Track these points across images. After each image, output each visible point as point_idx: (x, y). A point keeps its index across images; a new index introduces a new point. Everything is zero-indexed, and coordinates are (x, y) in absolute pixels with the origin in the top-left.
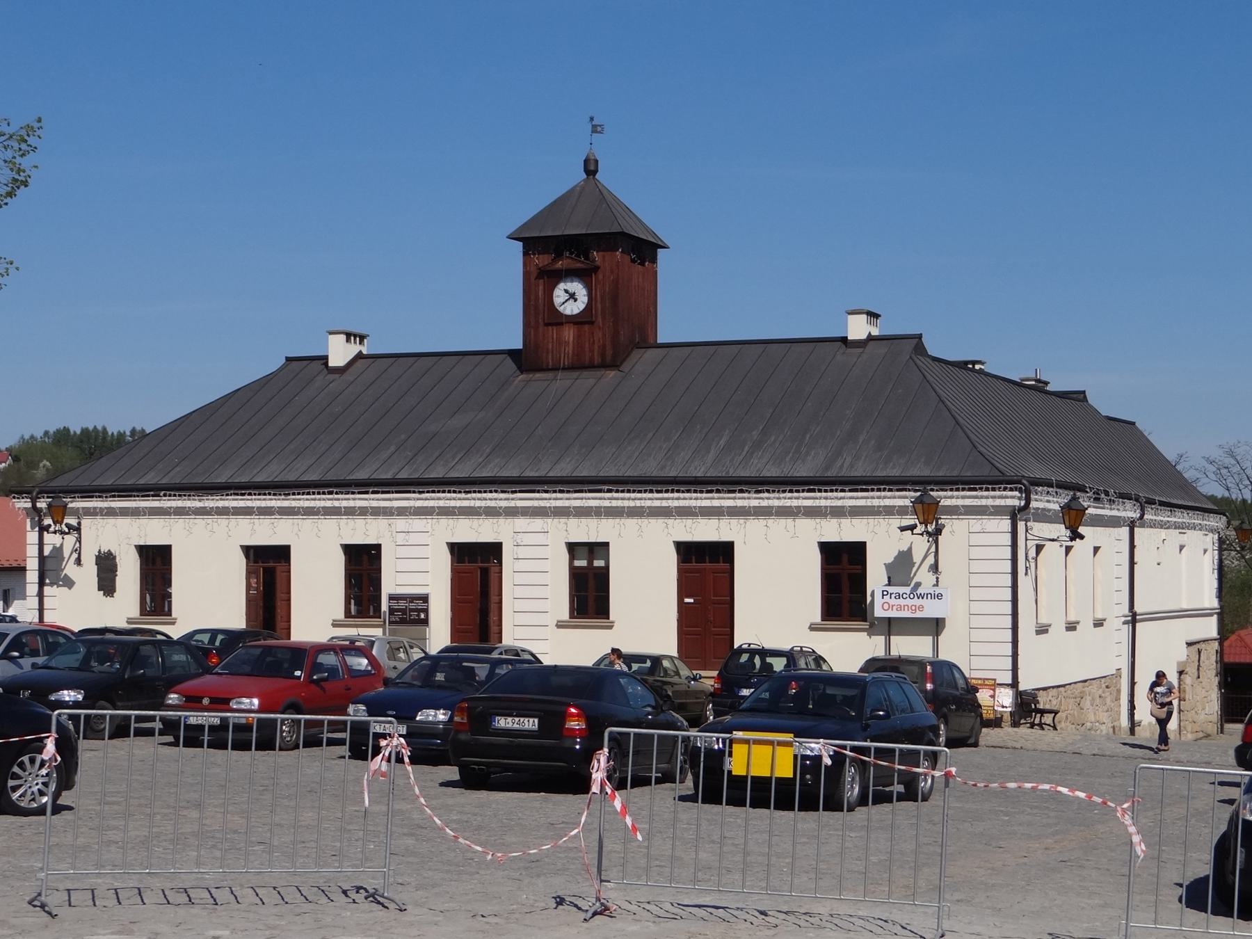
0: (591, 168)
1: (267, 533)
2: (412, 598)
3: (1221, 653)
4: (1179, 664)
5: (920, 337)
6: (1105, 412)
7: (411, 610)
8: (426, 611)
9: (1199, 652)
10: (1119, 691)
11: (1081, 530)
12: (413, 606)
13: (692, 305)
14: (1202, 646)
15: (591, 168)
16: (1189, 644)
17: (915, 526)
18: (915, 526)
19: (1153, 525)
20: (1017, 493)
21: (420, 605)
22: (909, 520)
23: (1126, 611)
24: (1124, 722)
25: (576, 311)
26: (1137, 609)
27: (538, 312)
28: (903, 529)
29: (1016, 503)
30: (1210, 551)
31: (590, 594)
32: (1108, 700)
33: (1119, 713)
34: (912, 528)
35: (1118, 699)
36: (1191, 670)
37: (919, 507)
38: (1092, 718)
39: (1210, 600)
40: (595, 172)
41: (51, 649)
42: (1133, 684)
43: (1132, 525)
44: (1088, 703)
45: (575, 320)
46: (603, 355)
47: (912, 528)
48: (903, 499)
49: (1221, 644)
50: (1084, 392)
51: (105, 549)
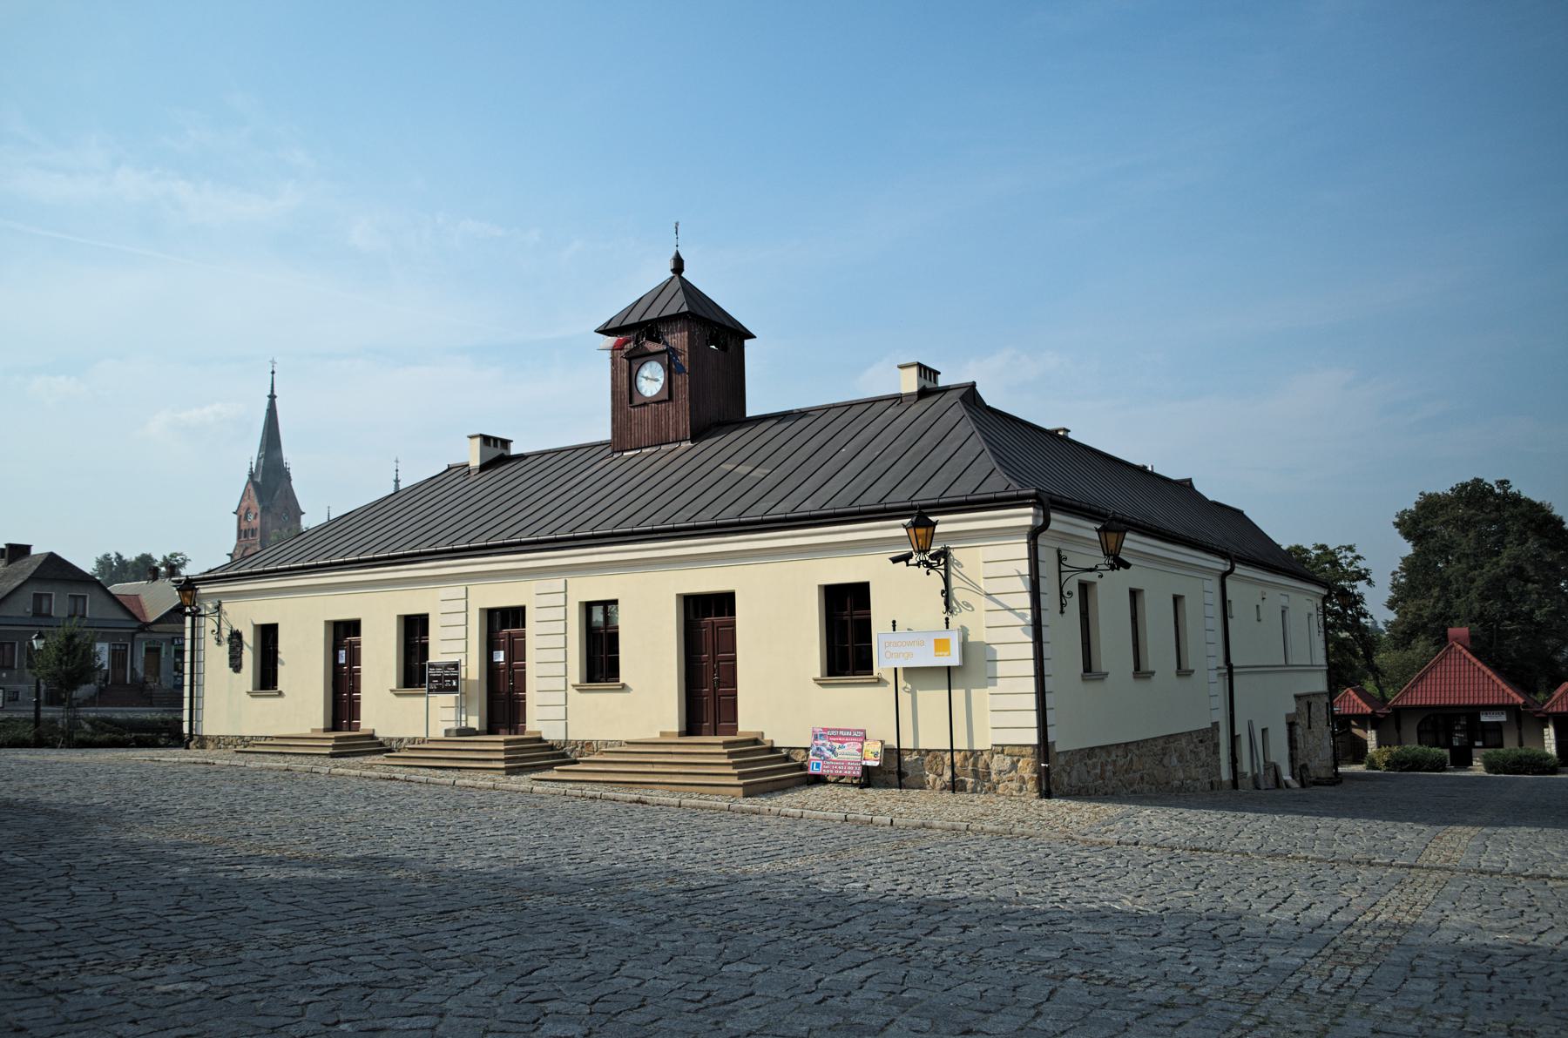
3: (1331, 705)
4: (1288, 716)
5: (974, 385)
8: (456, 678)
9: (1309, 705)
10: (1217, 745)
14: (1312, 699)
16: (1297, 697)
17: (909, 556)
18: (909, 556)
20: (1031, 510)
21: (451, 672)
23: (1222, 664)
24: (1226, 775)
26: (1233, 661)
27: (625, 395)
28: (895, 560)
30: (1314, 617)
31: (601, 657)
32: (1203, 756)
33: (1218, 768)
34: (906, 558)
35: (1216, 751)
36: (1303, 722)
37: (912, 531)
38: (1181, 775)
39: (1321, 659)
42: (1234, 739)
43: (1224, 575)
44: (1175, 759)
45: (657, 401)
46: (677, 431)
47: (906, 558)
48: (896, 529)
49: (1331, 699)
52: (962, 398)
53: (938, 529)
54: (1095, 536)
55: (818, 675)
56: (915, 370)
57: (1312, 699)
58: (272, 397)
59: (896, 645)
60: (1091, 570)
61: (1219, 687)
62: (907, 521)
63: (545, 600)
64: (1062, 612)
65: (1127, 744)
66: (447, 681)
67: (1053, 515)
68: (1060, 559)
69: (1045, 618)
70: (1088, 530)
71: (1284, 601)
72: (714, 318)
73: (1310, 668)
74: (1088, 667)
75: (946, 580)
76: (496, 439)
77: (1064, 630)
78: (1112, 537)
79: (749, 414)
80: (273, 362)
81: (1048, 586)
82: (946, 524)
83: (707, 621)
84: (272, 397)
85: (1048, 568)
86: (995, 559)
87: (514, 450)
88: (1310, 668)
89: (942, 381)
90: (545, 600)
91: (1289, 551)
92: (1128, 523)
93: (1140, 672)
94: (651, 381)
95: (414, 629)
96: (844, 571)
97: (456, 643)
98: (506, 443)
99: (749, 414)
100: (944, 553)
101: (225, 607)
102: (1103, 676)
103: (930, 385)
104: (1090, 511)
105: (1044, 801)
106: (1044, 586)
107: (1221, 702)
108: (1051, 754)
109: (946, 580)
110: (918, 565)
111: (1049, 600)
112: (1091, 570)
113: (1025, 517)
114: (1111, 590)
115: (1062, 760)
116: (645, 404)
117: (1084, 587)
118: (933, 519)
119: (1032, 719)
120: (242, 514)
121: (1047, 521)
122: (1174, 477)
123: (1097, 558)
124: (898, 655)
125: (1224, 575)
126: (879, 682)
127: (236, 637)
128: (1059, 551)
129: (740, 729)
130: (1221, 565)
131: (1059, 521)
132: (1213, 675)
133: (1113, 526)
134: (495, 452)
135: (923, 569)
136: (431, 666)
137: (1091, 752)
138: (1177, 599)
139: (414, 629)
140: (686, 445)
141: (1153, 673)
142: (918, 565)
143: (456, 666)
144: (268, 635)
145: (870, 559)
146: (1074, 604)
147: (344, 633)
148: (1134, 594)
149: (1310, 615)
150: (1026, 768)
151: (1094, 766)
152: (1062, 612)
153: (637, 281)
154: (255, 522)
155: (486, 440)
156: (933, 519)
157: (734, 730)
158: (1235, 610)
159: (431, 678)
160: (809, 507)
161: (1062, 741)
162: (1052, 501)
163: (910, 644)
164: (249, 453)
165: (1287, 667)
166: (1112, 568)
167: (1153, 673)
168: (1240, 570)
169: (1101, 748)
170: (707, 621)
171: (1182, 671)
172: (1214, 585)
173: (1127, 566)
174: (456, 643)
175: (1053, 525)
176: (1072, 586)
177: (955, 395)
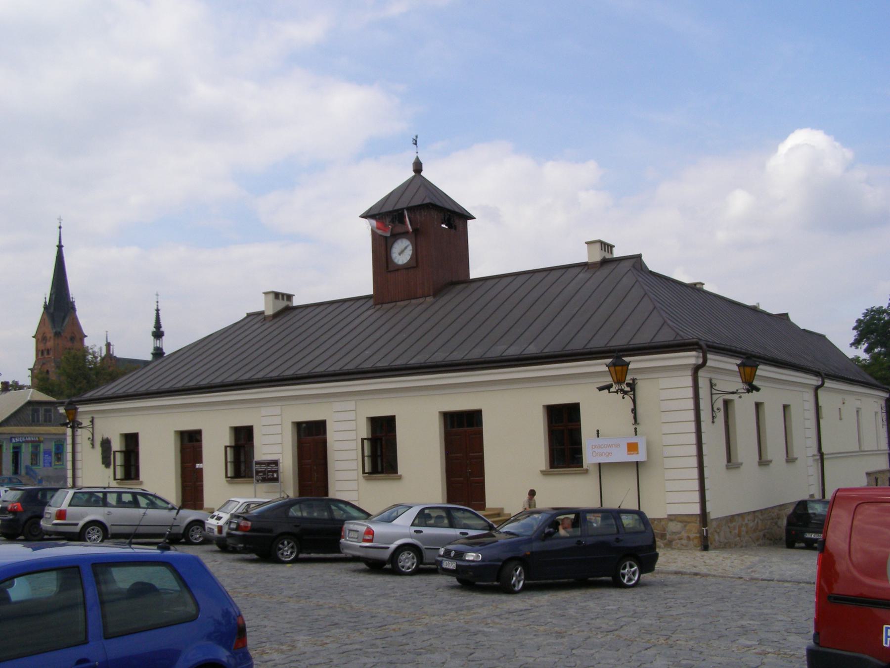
0: (418, 167)
1: (189, 423)
2: (269, 463)
5: (639, 257)
6: (802, 328)
7: (269, 472)
8: (277, 471)
9: (877, 479)
11: (755, 383)
12: (269, 468)
13: (490, 254)
15: (418, 167)
16: (868, 474)
17: (611, 386)
19: (831, 390)
20: (694, 353)
21: (274, 468)
22: (608, 380)
25: (405, 261)
26: (824, 450)
29: (693, 361)
30: (880, 414)
34: (608, 387)
37: (612, 369)
40: (421, 170)
41: (152, 505)
43: (817, 388)
45: (406, 267)
47: (608, 387)
48: (601, 366)
50: (787, 314)
51: (105, 437)
52: (634, 266)
53: (630, 367)
54: (736, 368)
55: (544, 468)
56: (598, 246)
57: (878, 476)
58: (60, 247)
59: (600, 447)
60: (733, 393)
61: (814, 470)
62: (609, 361)
63: (342, 416)
64: (713, 422)
65: (754, 512)
66: (269, 473)
67: (709, 356)
68: (712, 386)
69: (703, 429)
70: (732, 364)
71: (858, 404)
72: (448, 207)
73: (875, 453)
74: (729, 460)
75: (634, 401)
76: (283, 295)
77: (713, 434)
78: (748, 370)
79: (471, 277)
80: (60, 219)
81: (705, 405)
82: (636, 363)
83: (463, 434)
84: (60, 247)
85: (704, 392)
86: (667, 385)
87: (296, 302)
88: (875, 453)
89: (617, 253)
90: (342, 416)
91: (852, 360)
92: (760, 357)
93: (763, 462)
94: (402, 253)
95: (243, 438)
96: (562, 396)
97: (275, 444)
98: (289, 297)
99: (471, 277)
100: (632, 386)
101: (96, 421)
102: (738, 466)
103: (608, 256)
104: (730, 350)
105: (705, 553)
106: (702, 406)
107: (815, 480)
108: (708, 520)
109: (634, 401)
110: (617, 392)
111: (705, 415)
112: (733, 393)
113: (691, 358)
114: (744, 405)
115: (714, 524)
116: (397, 270)
117: (726, 403)
118: (626, 359)
119: (696, 497)
120: (40, 337)
121: (705, 361)
122: (774, 313)
123: (737, 384)
124: (601, 454)
125: (817, 388)
126: (586, 471)
127: (106, 444)
128: (711, 380)
129: (488, 506)
130: (815, 381)
131: (713, 360)
132: (810, 461)
133: (750, 363)
134: (282, 304)
135: (620, 395)
136: (258, 463)
137: (732, 518)
138: (786, 407)
139: (243, 438)
140: (430, 299)
141: (771, 461)
142: (617, 392)
143: (276, 463)
144: (131, 441)
145: (580, 384)
146: (720, 416)
147: (190, 444)
148: (758, 405)
149: (876, 413)
150: (694, 529)
151: (734, 528)
152: (713, 422)
153: (386, 179)
154: (50, 344)
155: (277, 295)
156: (626, 359)
157: (482, 507)
158: (824, 412)
159: (257, 472)
160: (532, 350)
161: (715, 511)
162: (708, 346)
163: (610, 446)
164: (44, 291)
165: (861, 453)
166: (748, 391)
167: (771, 461)
168: (828, 384)
169: (738, 515)
170: (463, 434)
171: (790, 459)
172: (809, 396)
173: (758, 390)
174: (275, 444)
175: (709, 363)
176: (719, 404)
177: (627, 264)
